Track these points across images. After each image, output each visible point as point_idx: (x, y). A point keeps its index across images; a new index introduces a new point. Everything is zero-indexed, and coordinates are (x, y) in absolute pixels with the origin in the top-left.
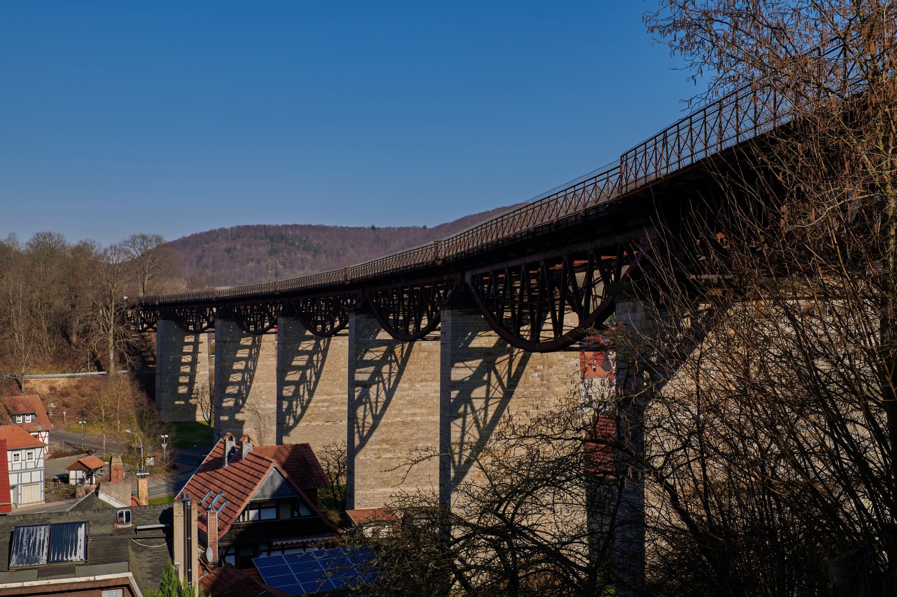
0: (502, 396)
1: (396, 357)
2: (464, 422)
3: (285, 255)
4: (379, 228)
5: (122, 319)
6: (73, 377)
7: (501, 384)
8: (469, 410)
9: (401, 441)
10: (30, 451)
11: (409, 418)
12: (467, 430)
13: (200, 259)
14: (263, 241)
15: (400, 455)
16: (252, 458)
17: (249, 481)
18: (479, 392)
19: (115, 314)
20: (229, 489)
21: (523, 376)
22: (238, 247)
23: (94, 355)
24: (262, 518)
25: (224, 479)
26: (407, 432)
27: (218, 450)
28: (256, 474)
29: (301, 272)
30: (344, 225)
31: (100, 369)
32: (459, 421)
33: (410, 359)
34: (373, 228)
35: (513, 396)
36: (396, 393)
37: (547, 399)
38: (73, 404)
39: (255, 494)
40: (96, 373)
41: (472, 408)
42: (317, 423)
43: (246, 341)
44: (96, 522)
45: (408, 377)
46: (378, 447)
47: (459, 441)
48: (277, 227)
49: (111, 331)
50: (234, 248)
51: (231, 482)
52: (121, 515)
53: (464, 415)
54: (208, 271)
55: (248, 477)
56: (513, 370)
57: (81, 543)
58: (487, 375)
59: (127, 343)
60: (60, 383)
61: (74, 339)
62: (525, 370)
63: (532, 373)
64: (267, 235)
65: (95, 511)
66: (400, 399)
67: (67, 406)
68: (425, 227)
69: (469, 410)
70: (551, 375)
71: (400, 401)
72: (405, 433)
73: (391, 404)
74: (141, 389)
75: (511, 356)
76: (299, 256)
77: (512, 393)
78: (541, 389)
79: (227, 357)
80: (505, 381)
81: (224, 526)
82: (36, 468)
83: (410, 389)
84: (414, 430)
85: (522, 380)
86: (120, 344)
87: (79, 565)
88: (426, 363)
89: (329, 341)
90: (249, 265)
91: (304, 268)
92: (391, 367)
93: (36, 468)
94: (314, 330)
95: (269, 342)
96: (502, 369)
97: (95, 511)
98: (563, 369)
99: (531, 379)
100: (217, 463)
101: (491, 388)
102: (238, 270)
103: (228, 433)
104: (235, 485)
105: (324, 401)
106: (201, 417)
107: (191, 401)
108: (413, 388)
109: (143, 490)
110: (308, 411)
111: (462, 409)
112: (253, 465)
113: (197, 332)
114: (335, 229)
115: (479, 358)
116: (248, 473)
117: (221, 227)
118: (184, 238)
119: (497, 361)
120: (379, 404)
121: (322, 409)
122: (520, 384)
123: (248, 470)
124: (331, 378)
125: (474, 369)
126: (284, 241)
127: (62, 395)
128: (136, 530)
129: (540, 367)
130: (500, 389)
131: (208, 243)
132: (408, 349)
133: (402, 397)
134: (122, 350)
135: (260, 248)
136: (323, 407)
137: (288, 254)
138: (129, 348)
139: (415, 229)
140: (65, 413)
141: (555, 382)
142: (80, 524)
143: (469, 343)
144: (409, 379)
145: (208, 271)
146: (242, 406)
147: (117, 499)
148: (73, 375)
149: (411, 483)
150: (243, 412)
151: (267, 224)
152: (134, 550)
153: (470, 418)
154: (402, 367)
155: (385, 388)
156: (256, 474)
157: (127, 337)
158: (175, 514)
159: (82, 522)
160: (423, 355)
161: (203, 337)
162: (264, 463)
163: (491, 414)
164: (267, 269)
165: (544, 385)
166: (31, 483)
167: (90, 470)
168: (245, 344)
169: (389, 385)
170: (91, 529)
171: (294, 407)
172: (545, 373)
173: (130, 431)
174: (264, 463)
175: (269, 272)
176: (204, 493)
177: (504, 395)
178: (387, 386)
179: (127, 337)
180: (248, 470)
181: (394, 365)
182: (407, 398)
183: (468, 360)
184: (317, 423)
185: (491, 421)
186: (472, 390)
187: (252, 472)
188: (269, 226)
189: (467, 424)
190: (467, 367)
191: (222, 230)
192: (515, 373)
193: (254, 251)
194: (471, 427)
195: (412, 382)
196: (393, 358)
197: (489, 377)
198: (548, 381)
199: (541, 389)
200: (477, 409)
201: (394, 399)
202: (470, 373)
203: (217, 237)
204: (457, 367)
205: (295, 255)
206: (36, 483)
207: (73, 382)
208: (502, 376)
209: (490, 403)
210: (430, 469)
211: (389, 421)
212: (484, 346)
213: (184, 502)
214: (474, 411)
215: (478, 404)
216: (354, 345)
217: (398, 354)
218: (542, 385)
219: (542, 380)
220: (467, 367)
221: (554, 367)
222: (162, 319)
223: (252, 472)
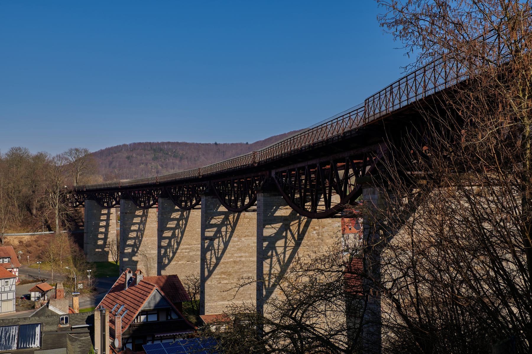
0: (294, 245)
1: (230, 222)
2: (271, 261)
3: (163, 160)
4: (219, 144)
5: (64, 200)
6: (34, 235)
7: (294, 238)
8: (274, 254)
9: (233, 273)
10: (7, 280)
11: (238, 259)
12: (273, 266)
13: (111, 163)
14: (149, 152)
15: (232, 281)
16: (142, 284)
17: (140, 298)
18: (280, 243)
19: (59, 196)
20: (128, 302)
21: (307, 233)
22: (134, 155)
23: (46, 221)
24: (149, 320)
25: (125, 297)
26: (237, 267)
27: (122, 279)
28: (145, 293)
29: (172, 170)
30: (198, 142)
31: (50, 230)
32: (268, 261)
34: (216, 144)
37: (322, 247)
38: (33, 251)
39: (144, 306)
40: (48, 232)
41: (276, 253)
42: (182, 262)
43: (139, 213)
44: (47, 324)
45: (237, 234)
46: (219, 276)
47: (268, 273)
48: (158, 143)
49: (57, 207)
50: (132, 156)
51: (129, 299)
52: (62, 319)
53: (271, 257)
54: (116, 170)
55: (140, 295)
56: (301, 230)
57: (38, 337)
58: (285, 232)
59: (67, 214)
60: (25, 239)
61: (34, 212)
62: (308, 230)
64: (151, 148)
65: (46, 316)
66: (233, 247)
67: (29, 253)
68: (247, 143)
69: (274, 254)
70: (323, 232)
71: (232, 249)
73: (227, 251)
74: (75, 242)
75: (300, 221)
76: (171, 161)
77: (300, 243)
79: (127, 222)
80: (296, 236)
81: (125, 325)
82: (10, 291)
83: (239, 241)
84: (241, 266)
85: (306, 235)
86: (62, 214)
87: (37, 350)
88: (248, 225)
89: (189, 212)
90: (141, 166)
91: (174, 168)
92: (227, 228)
93: (10, 291)
94: (180, 206)
95: (153, 213)
97: (46, 316)
98: (330, 229)
99: (312, 235)
100: (121, 287)
101: (288, 240)
102: (134, 169)
103: (128, 269)
104: (132, 300)
105: (186, 249)
106: (111, 259)
107: (105, 249)
108: (240, 241)
109: (76, 304)
110: (177, 255)
111: (270, 254)
112: (143, 288)
113: (109, 207)
114: (193, 144)
115: (280, 222)
116: (140, 293)
118: (101, 150)
119: (291, 224)
121: (185, 254)
122: (305, 238)
123: (140, 291)
124: (190, 235)
125: (277, 229)
126: (162, 152)
127: (27, 246)
128: (71, 328)
129: (317, 228)
130: (293, 241)
132: (237, 217)
134: (63, 218)
135: (147, 156)
136: (186, 252)
137: (165, 160)
138: (68, 217)
139: (241, 144)
140: (28, 257)
141: (326, 237)
142: (37, 325)
143: (274, 213)
144: (238, 235)
145: (116, 170)
146: (137, 252)
147: (60, 309)
148: (34, 233)
149: (239, 298)
150: (137, 256)
151: (152, 141)
152: (70, 340)
153: (275, 259)
154: (233, 228)
155: (223, 241)
156: (145, 293)
157: (67, 211)
158: (95, 318)
159: (39, 324)
160: (246, 221)
161: (113, 210)
162: (150, 287)
163: (287, 256)
164: (152, 169)
166: (8, 300)
167: (44, 291)
168: (138, 214)
169: (226, 239)
170: (44, 328)
171: (168, 252)
172: (320, 231)
173: (69, 268)
174: (150, 287)
175: (153, 170)
176: (113, 305)
177: (295, 245)
178: (224, 240)
179: (67, 211)
180: (140, 291)
181: (229, 226)
182: (237, 247)
183: (273, 224)
184: (182, 262)
185: (287, 260)
186: (276, 242)
187: (143, 292)
188: (153, 143)
189: (273, 262)
190: (273, 227)
191: (125, 145)
192: (302, 231)
193: (144, 158)
195: (239, 237)
196: (228, 223)
197: (286, 233)
198: (322, 236)
200: (279, 253)
201: (229, 247)
202: (275, 231)
203: (121, 149)
204: (267, 228)
206: (10, 300)
207: (34, 238)
208: (294, 233)
209: (287, 249)
210: (251, 290)
211: (226, 261)
212: (283, 215)
213: (101, 311)
215: (280, 250)
216: (205, 215)
217: (231, 220)
219: (318, 235)
220: (273, 227)
222: (88, 199)
223: (143, 292)
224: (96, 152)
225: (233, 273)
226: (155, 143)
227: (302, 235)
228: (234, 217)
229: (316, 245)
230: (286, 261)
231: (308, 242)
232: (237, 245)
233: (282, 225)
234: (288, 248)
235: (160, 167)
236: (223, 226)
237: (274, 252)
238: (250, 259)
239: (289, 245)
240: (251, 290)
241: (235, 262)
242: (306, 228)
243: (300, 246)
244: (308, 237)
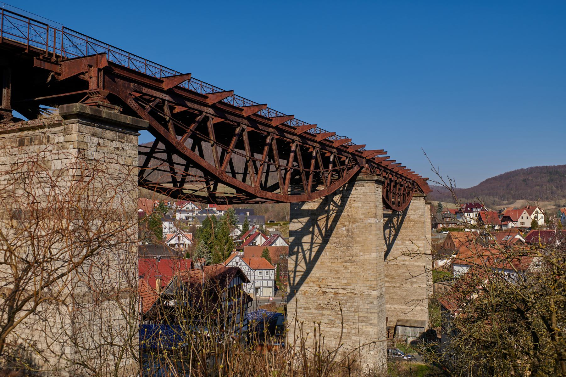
0: (321, 242)
1: (393, 224)
2: (297, 258)
7: (321, 234)
8: (300, 250)
9: (396, 276)
10: (267, 271)
12: (298, 263)
13: (508, 186)
14: (545, 175)
18: (307, 239)
21: (335, 229)
22: (530, 178)
32: (294, 257)
33: (402, 226)
35: (329, 242)
36: (393, 247)
37: (351, 245)
41: (302, 249)
45: (401, 237)
47: (293, 270)
48: (554, 167)
53: (297, 253)
56: (329, 225)
62: (337, 226)
66: (396, 250)
69: (300, 250)
70: (354, 229)
71: (395, 252)
72: (399, 272)
73: (390, 253)
75: (328, 216)
78: (347, 239)
80: (323, 232)
82: (270, 280)
83: (402, 245)
85: (334, 232)
88: (413, 229)
92: (390, 231)
93: (270, 280)
96: (322, 224)
98: (362, 225)
99: (340, 231)
101: (314, 236)
102: (529, 191)
108: (404, 244)
111: (296, 250)
118: (501, 175)
119: (318, 219)
120: (297, 274)
122: (333, 235)
125: (304, 224)
130: (320, 237)
131: (514, 177)
133: (397, 249)
135: (543, 179)
137: (560, 181)
141: (356, 234)
143: (301, 207)
144: (401, 238)
151: (548, 165)
153: (300, 256)
160: (411, 224)
163: (313, 254)
164: (547, 190)
166: (268, 287)
169: (389, 241)
172: (350, 227)
177: (322, 241)
178: (388, 242)
181: (392, 229)
183: (300, 218)
186: (302, 237)
188: (550, 166)
189: (298, 259)
190: (299, 222)
191: (522, 170)
192: (330, 227)
194: (301, 262)
195: (403, 240)
196: (392, 225)
197: (313, 229)
198: (352, 233)
199: (347, 239)
200: (305, 250)
201: (392, 250)
202: (302, 226)
204: (294, 222)
205: (564, 181)
206: (270, 287)
208: (321, 229)
209: (313, 246)
210: (415, 296)
212: (311, 208)
214: (303, 251)
215: (306, 247)
217: (395, 223)
218: (347, 236)
219: (348, 232)
220: (299, 222)
221: (357, 224)
224: (496, 177)
225: (396, 276)
226: (552, 166)
228: (398, 220)
229: (345, 243)
231: (337, 239)
233: (309, 219)
234: (314, 244)
235: (555, 188)
236: (387, 229)
238: (415, 263)
239: (316, 242)
240: (415, 296)
242: (334, 224)
243: (327, 243)
244: (336, 234)
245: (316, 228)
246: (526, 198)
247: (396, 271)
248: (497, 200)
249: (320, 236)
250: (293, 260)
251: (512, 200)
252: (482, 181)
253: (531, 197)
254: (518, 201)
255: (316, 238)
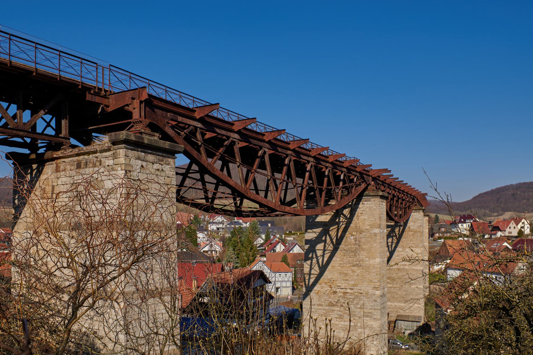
0: (332, 249)
1: (395, 234)
2: (311, 263)
7: (332, 242)
8: (314, 256)
10: (286, 273)
12: (313, 267)
15: (396, 286)
18: (320, 246)
21: (345, 238)
22: (519, 193)
26: (400, 274)
32: (309, 262)
33: (403, 236)
36: (395, 253)
41: (316, 255)
45: (402, 245)
47: (308, 273)
56: (339, 235)
58: (324, 237)
62: (346, 235)
63: (350, 237)
66: (397, 256)
69: (314, 256)
71: (397, 258)
73: (392, 259)
75: (338, 227)
77: (338, 248)
80: (334, 241)
82: (288, 281)
83: (403, 251)
84: (404, 273)
85: (344, 240)
88: (412, 238)
92: (393, 239)
93: (288, 281)
98: (368, 235)
99: (349, 240)
101: (327, 244)
111: (310, 256)
117: (511, 184)
120: (312, 276)
122: (343, 243)
125: (318, 234)
129: (354, 233)
130: (331, 245)
131: (503, 192)
132: (402, 230)
133: (398, 256)
141: (363, 242)
144: (402, 246)
153: (314, 260)
163: (325, 259)
165: (357, 244)
166: (286, 287)
178: (390, 249)
181: (394, 238)
182: (401, 256)
183: (314, 229)
185: (326, 263)
186: (316, 245)
189: (313, 264)
190: (313, 232)
191: (512, 185)
192: (340, 236)
196: (394, 235)
197: (326, 238)
198: (359, 241)
200: (318, 256)
202: (316, 236)
206: (288, 287)
209: (326, 253)
210: (413, 295)
212: (323, 220)
214: (317, 257)
215: (319, 253)
217: (397, 233)
219: (356, 241)
220: (313, 232)
227: (340, 240)
228: (399, 230)
230: (324, 264)
232: (401, 255)
237: (314, 254)
239: (328, 249)
240: (413, 295)
241: (398, 269)
243: (337, 250)
244: (346, 242)
245: (328, 238)
246: (514, 211)
247: (397, 274)
248: (487, 212)
249: (331, 244)
250: (308, 265)
251: (501, 212)
252: (475, 195)
253: (518, 209)
254: (506, 213)
255: (328, 246)
